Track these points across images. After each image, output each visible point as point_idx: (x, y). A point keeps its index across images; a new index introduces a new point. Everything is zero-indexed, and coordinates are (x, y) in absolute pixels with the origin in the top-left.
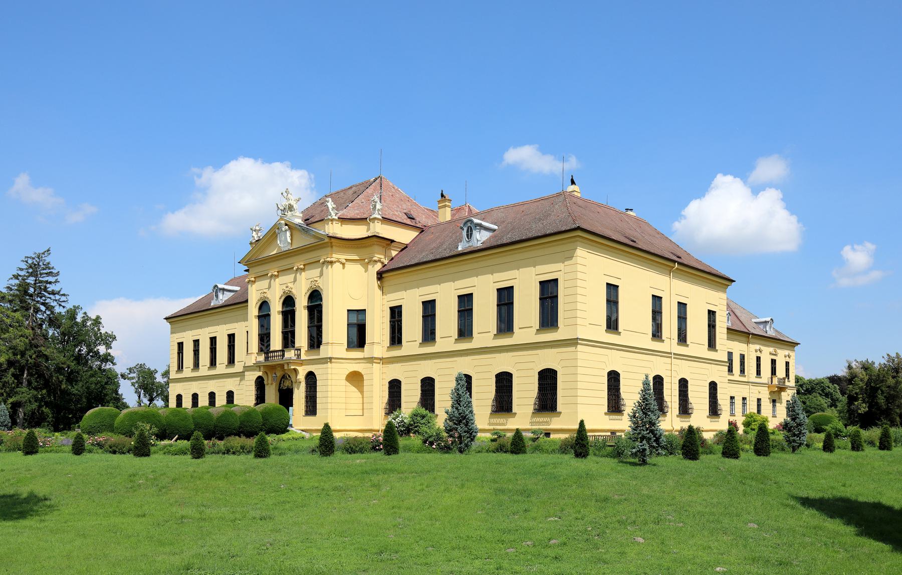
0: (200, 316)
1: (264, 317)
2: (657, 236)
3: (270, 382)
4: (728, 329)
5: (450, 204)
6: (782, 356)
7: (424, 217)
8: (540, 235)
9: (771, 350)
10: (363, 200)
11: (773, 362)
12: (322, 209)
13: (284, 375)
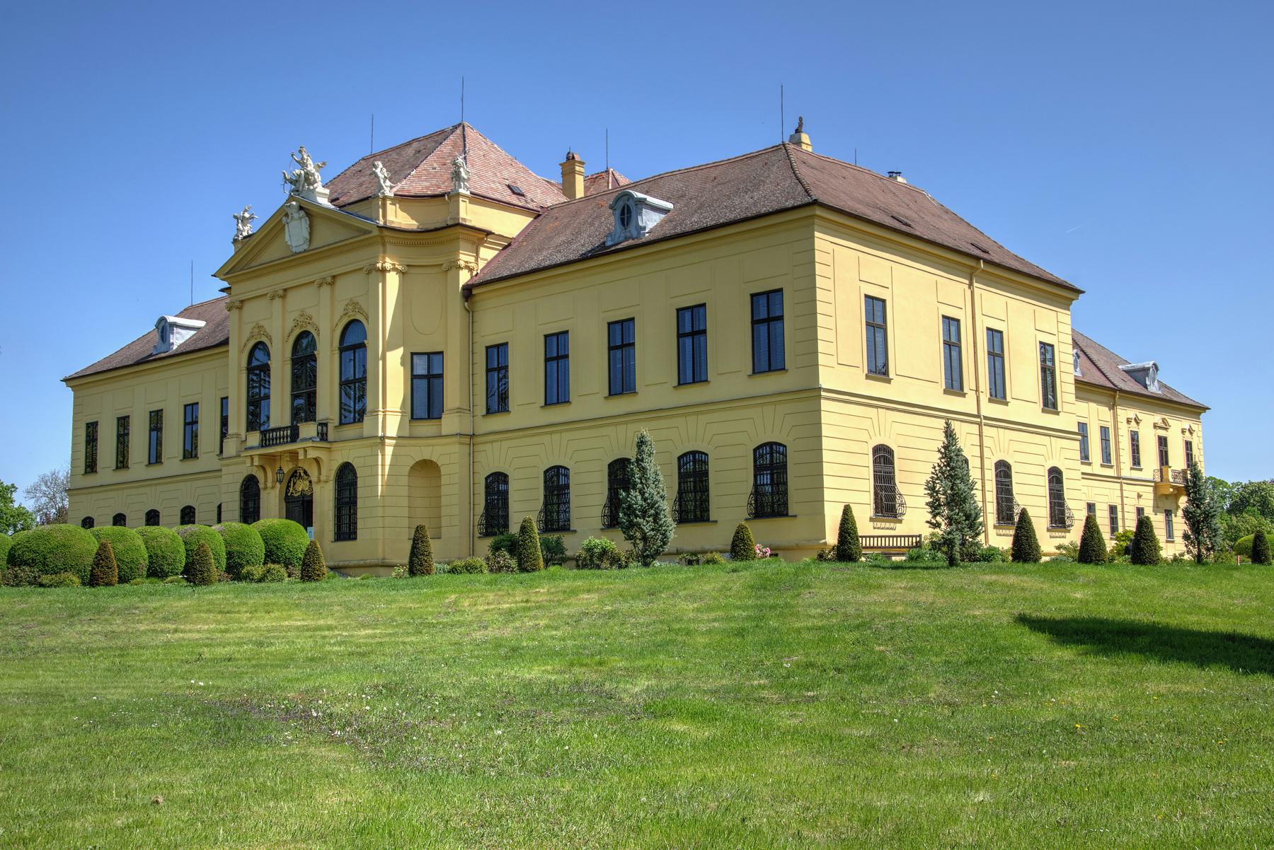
0: (131, 373)
1: (258, 372)
2: (945, 217)
3: (269, 485)
4: (1077, 381)
5: (582, 170)
6: (1177, 427)
7: (539, 191)
8: (749, 215)
9: (1158, 418)
10: (435, 165)
11: (1163, 442)
12: (360, 180)
13: (296, 472)
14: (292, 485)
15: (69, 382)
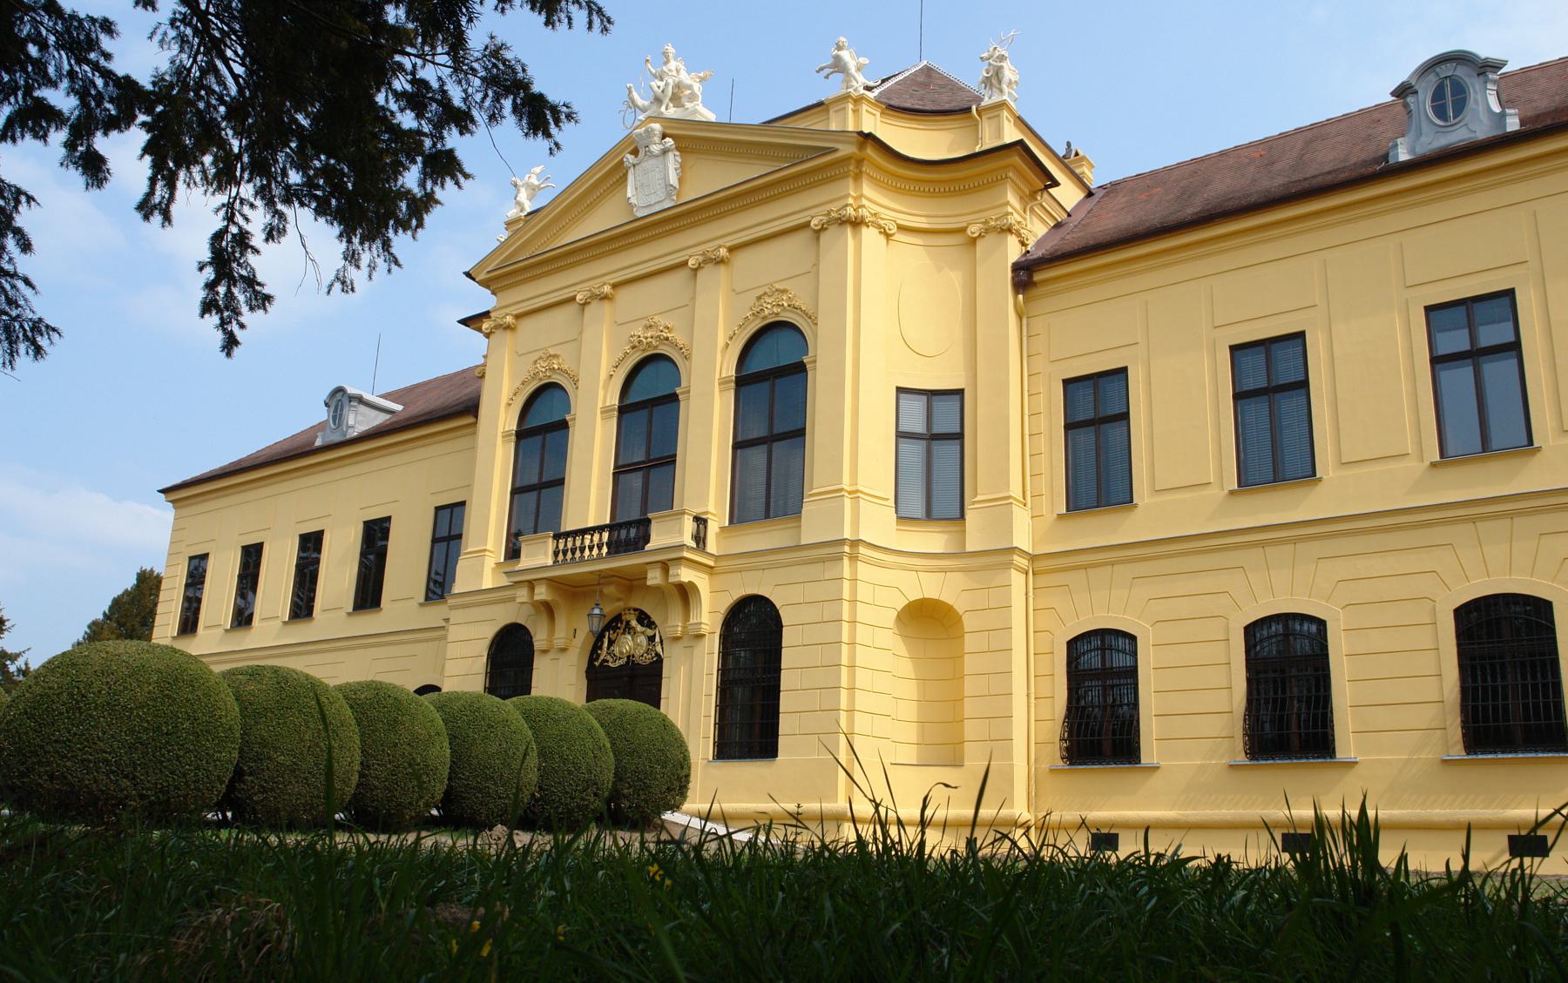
14: (606, 644)
15: (170, 494)
